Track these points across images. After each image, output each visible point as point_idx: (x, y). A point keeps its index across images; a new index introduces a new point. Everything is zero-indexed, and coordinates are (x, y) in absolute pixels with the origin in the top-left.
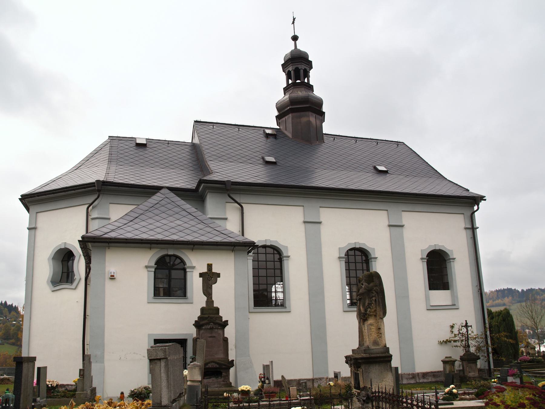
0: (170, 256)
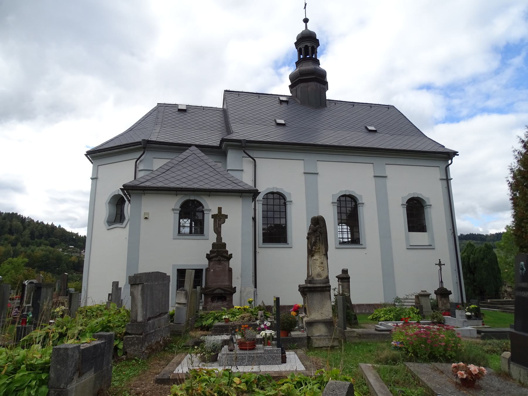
0: (192, 201)
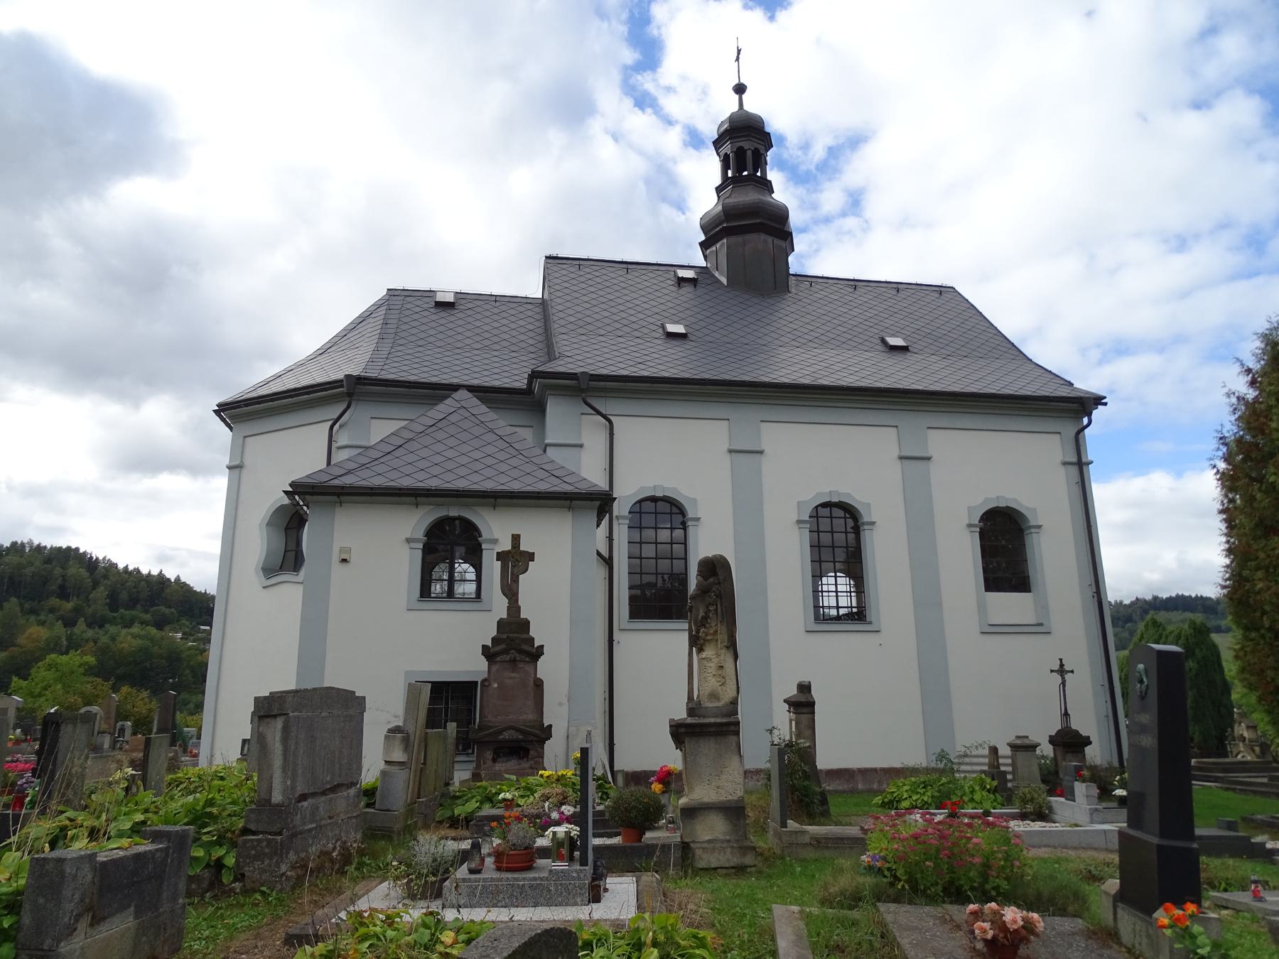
0: (454, 519)
